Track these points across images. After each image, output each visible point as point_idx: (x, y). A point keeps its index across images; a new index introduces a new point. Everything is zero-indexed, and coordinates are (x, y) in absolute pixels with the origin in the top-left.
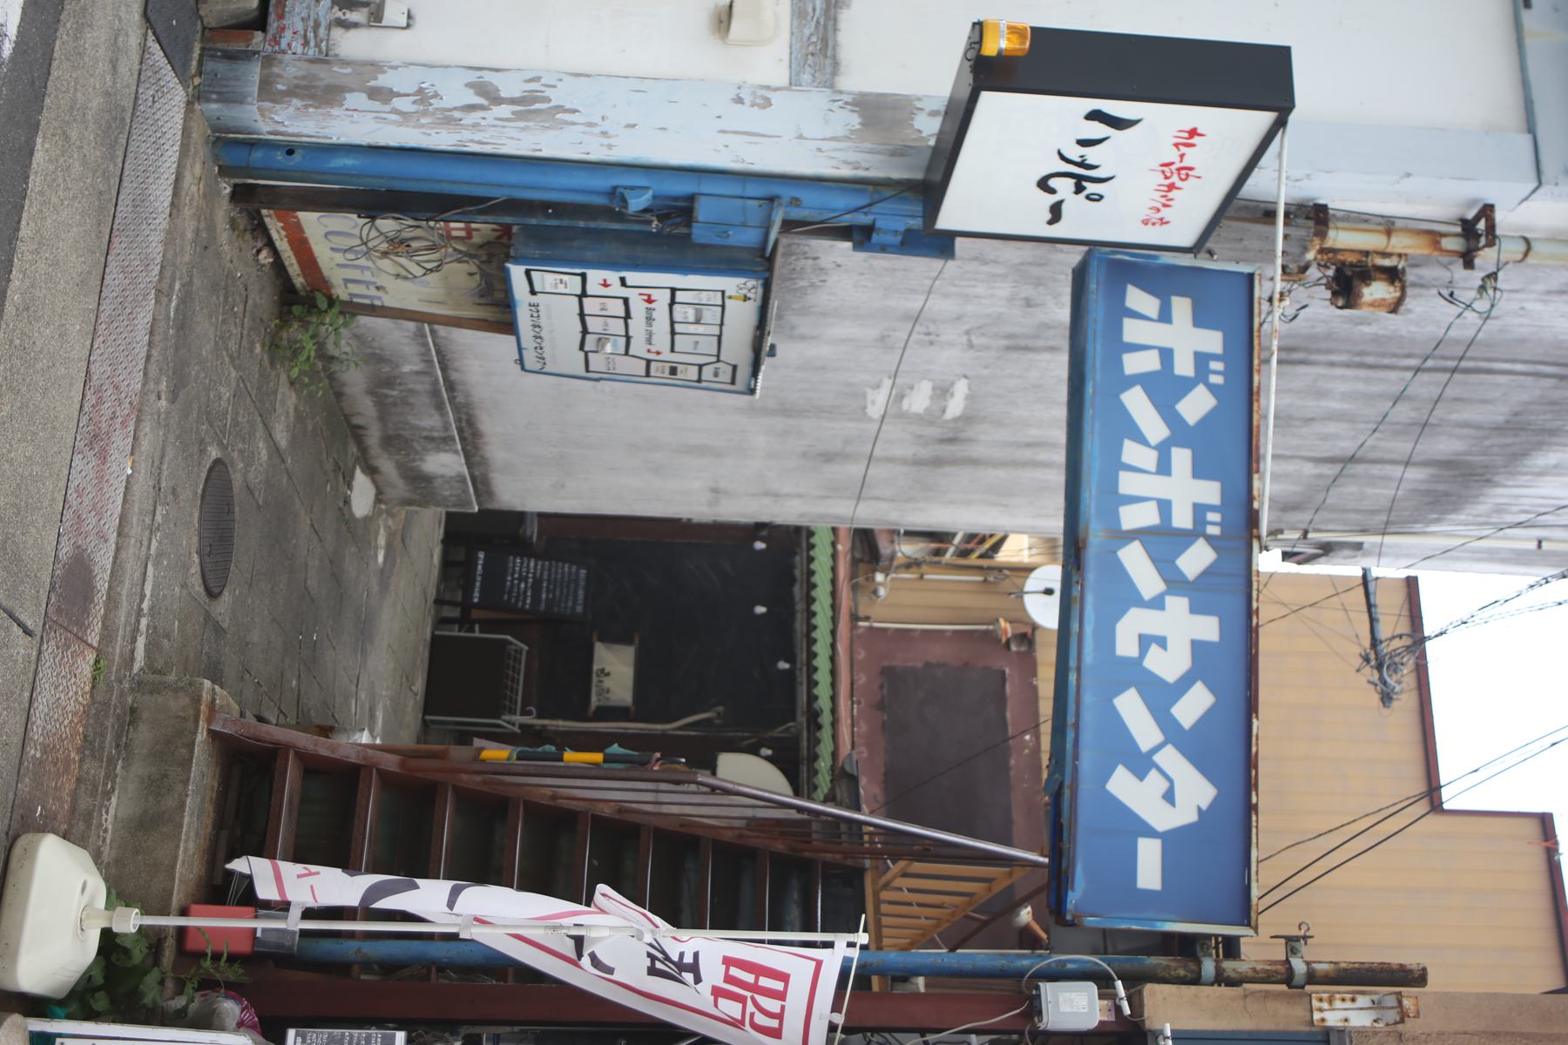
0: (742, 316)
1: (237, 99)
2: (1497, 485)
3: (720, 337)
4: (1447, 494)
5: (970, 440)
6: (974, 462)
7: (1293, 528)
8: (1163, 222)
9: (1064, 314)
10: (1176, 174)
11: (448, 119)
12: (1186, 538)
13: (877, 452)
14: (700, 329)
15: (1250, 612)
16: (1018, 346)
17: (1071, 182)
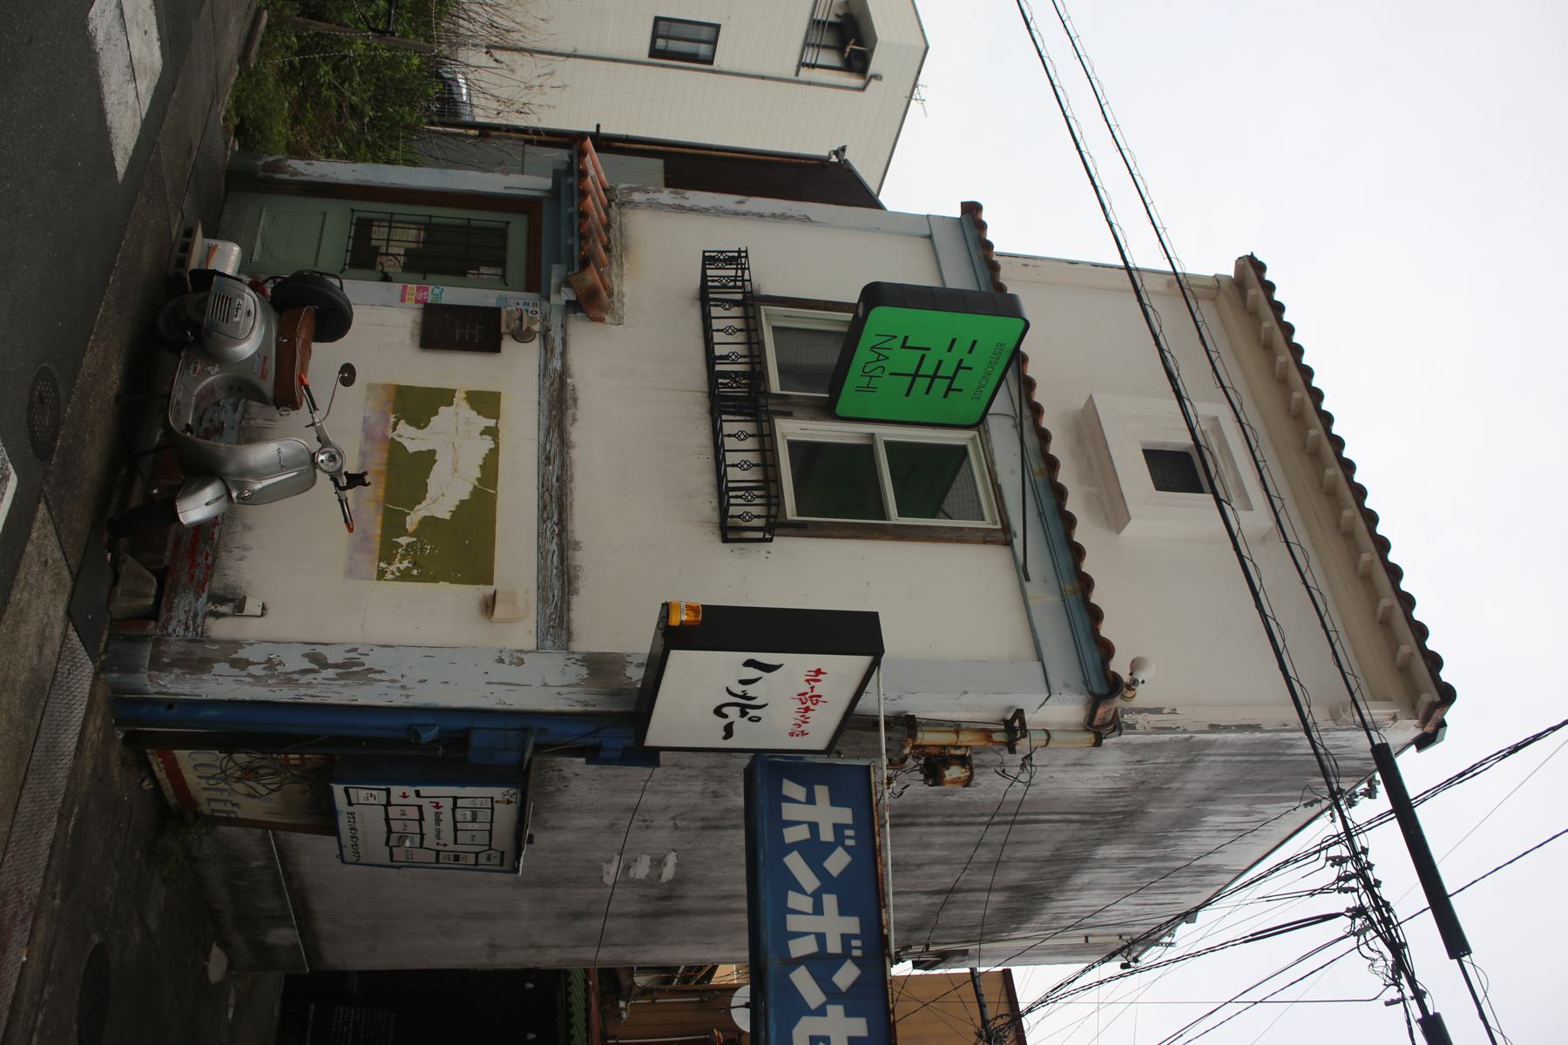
0: (505, 815)
1: (134, 669)
2: (1052, 900)
3: (490, 831)
4: (1021, 910)
5: (681, 897)
6: (686, 913)
7: (919, 944)
8: (803, 734)
9: (740, 801)
10: (809, 701)
11: (288, 680)
12: (837, 961)
13: (612, 909)
14: (476, 826)
15: (888, 1012)
16: (710, 826)
17: (737, 709)
